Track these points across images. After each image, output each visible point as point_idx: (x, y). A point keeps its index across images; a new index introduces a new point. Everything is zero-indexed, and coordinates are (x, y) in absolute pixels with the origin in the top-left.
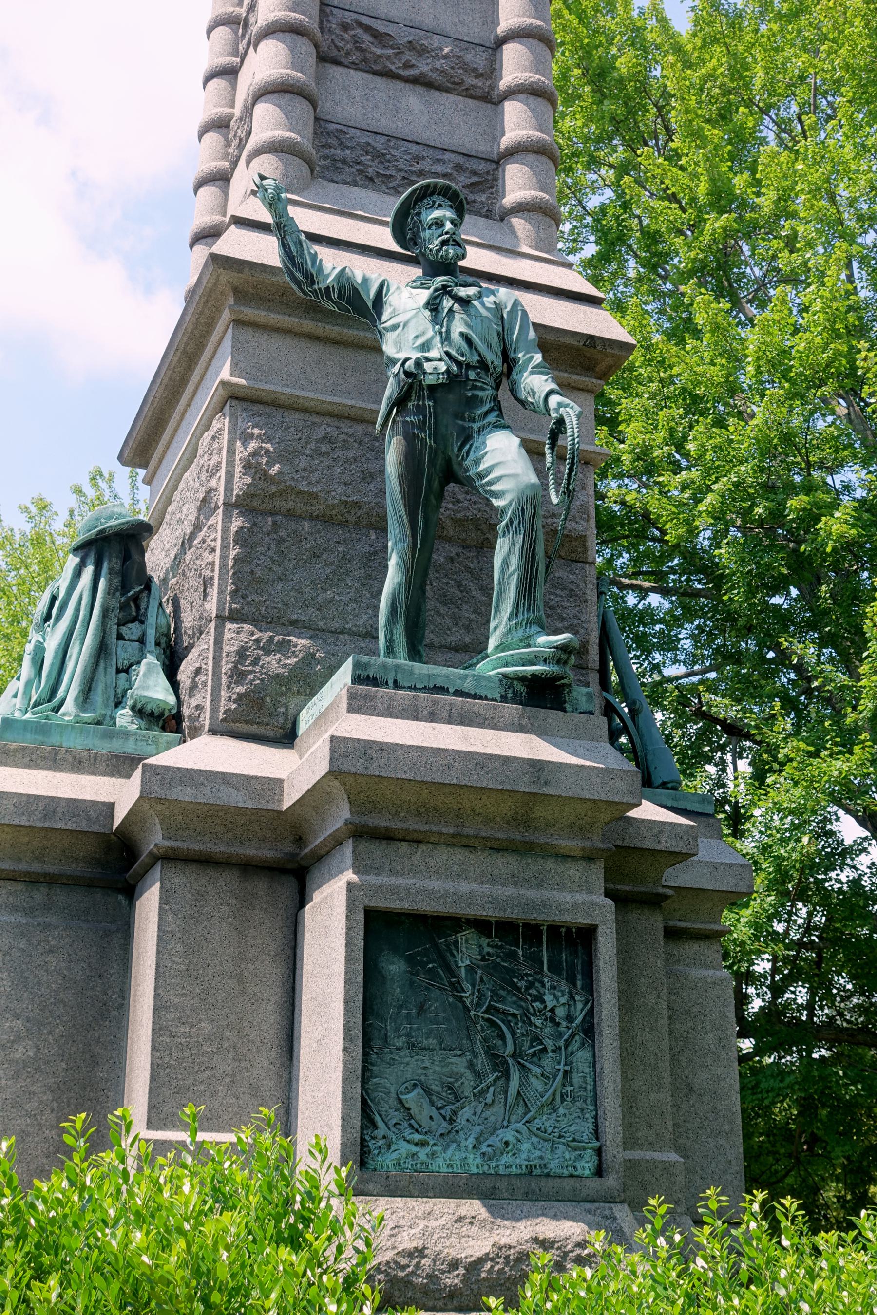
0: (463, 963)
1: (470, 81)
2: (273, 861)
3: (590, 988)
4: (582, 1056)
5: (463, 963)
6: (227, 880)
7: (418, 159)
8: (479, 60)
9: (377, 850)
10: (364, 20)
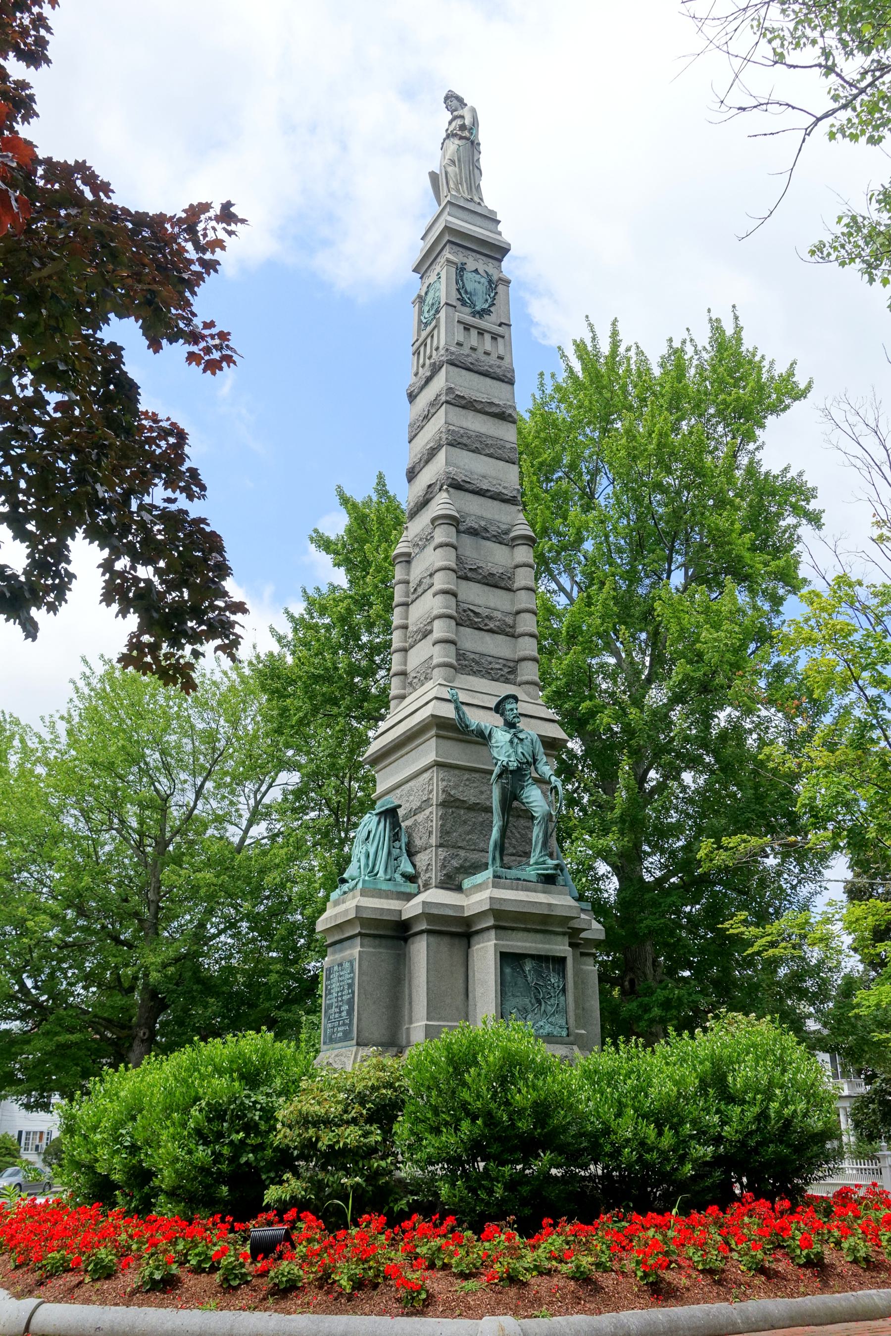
0: (527, 969)
1: (508, 630)
2: (459, 932)
3: (564, 977)
4: (562, 998)
5: (527, 969)
6: (446, 940)
7: (490, 663)
8: (509, 620)
9: (502, 932)
10: (472, 607)
